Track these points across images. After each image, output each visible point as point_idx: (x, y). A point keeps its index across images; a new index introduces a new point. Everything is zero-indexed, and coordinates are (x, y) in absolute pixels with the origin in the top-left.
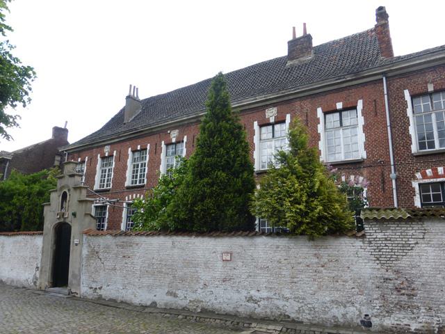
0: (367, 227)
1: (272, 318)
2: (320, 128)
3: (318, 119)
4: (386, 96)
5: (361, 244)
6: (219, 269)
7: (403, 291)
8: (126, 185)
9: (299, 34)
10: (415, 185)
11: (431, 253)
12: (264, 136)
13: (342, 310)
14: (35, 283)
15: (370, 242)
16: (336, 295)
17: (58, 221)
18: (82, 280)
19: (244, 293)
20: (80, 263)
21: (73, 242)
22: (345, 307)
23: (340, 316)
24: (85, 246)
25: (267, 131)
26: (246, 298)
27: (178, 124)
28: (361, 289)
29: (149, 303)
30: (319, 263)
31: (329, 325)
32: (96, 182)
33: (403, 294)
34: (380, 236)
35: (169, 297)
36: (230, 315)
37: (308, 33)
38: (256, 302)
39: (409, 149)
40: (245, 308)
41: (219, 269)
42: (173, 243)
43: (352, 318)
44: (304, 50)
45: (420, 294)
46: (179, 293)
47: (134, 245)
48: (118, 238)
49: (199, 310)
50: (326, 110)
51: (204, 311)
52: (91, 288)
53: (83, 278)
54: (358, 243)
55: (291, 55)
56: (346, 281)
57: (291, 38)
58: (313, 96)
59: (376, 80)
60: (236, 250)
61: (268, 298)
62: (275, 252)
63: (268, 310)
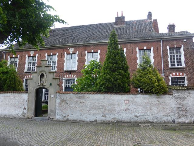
0: (173, 92)
1: (144, 122)
2: (65, 59)
3: (137, 52)
4: (161, 47)
5: (172, 97)
6: (124, 106)
7: (184, 111)
8: (65, 69)
9: (120, 15)
10: (170, 78)
11: (191, 99)
12: (89, 57)
13: (166, 118)
14: (23, 116)
15: (174, 96)
16: (165, 113)
17: (38, 87)
18: (56, 113)
19: (133, 114)
20: (55, 106)
21: (50, 97)
22: (167, 117)
23: (166, 120)
24: (58, 98)
25: (69, 56)
26: (134, 116)
27: (74, 46)
28: (172, 110)
29: (93, 120)
30: (158, 103)
31: (162, 123)
32: (26, 68)
33: (184, 112)
34: (177, 94)
35: (103, 117)
36: (128, 122)
37: (123, 16)
38: (138, 117)
39: (168, 66)
40: (134, 119)
41: (124, 106)
42: (104, 97)
43: (169, 120)
44: (122, 22)
45: (189, 112)
46: (107, 116)
47: (86, 98)
48: (77, 95)
49: (116, 122)
50: (140, 49)
51: (118, 122)
52: (62, 116)
53: (57, 112)
54: (171, 97)
55: (116, 23)
56: (167, 109)
57: (116, 16)
58: (135, 43)
59: (158, 41)
60: (130, 99)
61: (142, 116)
62: (144, 100)
63: (142, 120)
